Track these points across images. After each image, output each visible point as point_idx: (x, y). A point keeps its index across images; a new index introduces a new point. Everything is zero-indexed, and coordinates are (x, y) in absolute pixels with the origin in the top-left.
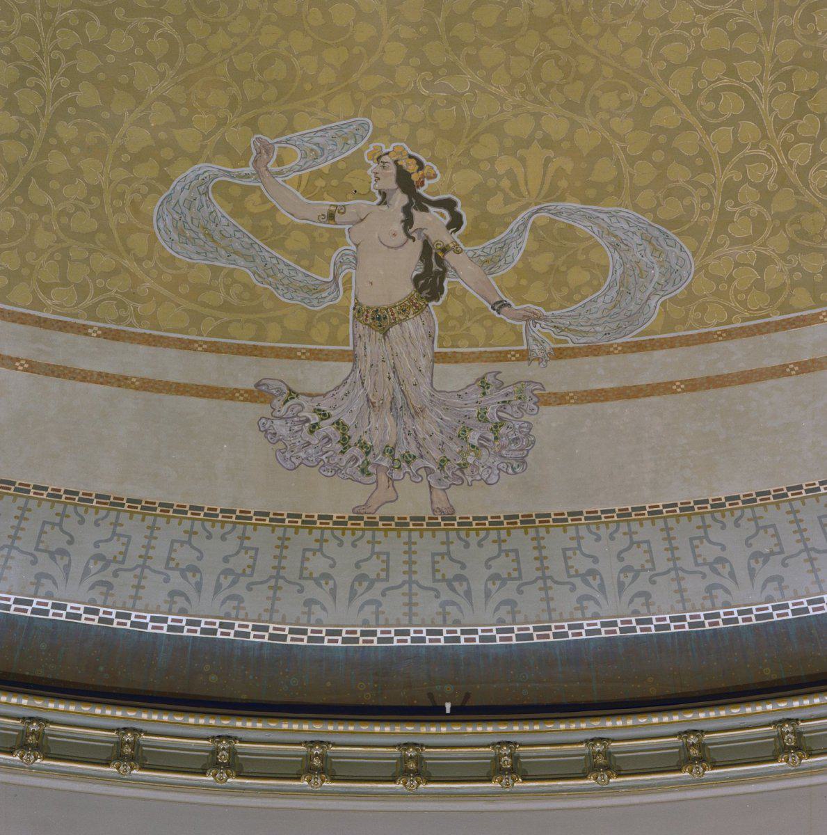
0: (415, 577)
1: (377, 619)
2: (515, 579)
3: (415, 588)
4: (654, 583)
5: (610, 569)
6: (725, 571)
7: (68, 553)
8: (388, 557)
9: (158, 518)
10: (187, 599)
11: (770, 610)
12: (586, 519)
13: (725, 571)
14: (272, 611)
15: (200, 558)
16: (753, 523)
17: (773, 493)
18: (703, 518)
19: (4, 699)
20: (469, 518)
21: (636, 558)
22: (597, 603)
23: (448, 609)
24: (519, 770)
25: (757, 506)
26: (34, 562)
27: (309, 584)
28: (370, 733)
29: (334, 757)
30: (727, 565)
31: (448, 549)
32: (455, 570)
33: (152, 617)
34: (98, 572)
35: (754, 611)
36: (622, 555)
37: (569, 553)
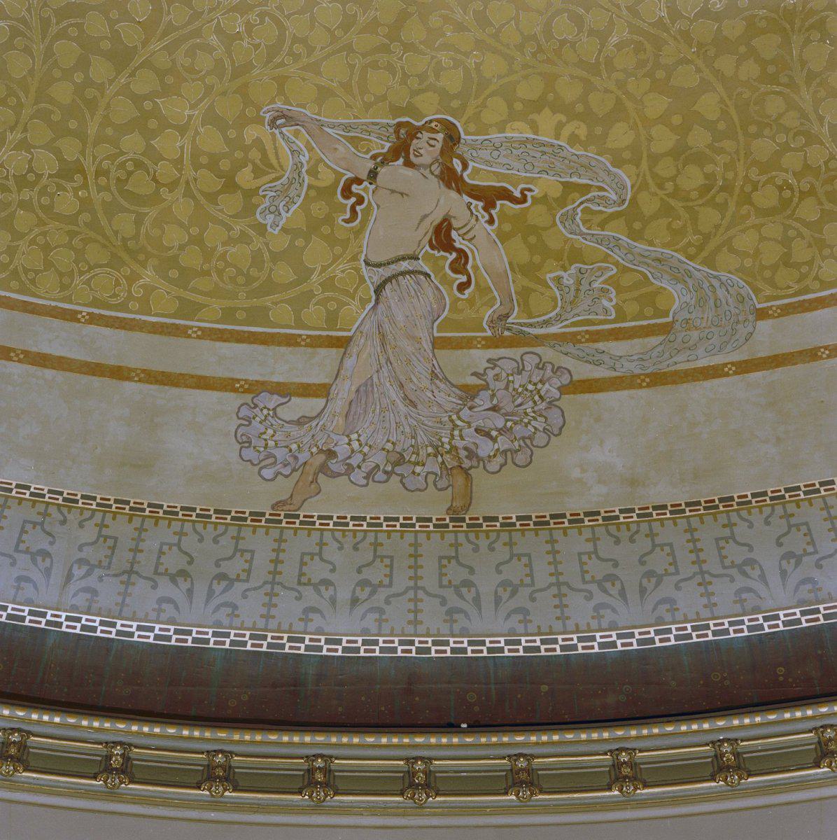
0: (420, 583)
1: (380, 628)
2: (527, 585)
3: (421, 594)
4: (533, 599)
5: (487, 584)
6: (756, 573)
7: (50, 554)
8: (392, 561)
9: (147, 520)
10: (177, 608)
11: (798, 616)
12: (671, 513)
13: (756, 573)
14: (267, 617)
15: (190, 563)
16: (508, 547)
17: (803, 489)
18: (728, 517)
19: (6, 712)
20: (780, 491)
21: (659, 562)
22: (614, 610)
23: (744, 596)
24: (230, 778)
25: (719, 513)
26: (13, 564)
27: (308, 592)
28: (476, 745)
29: (745, 753)
30: (473, 590)
31: (732, 533)
32: (463, 574)
33: (138, 625)
34: (83, 577)
35: (746, 622)
36: (500, 568)
37: (585, 558)
